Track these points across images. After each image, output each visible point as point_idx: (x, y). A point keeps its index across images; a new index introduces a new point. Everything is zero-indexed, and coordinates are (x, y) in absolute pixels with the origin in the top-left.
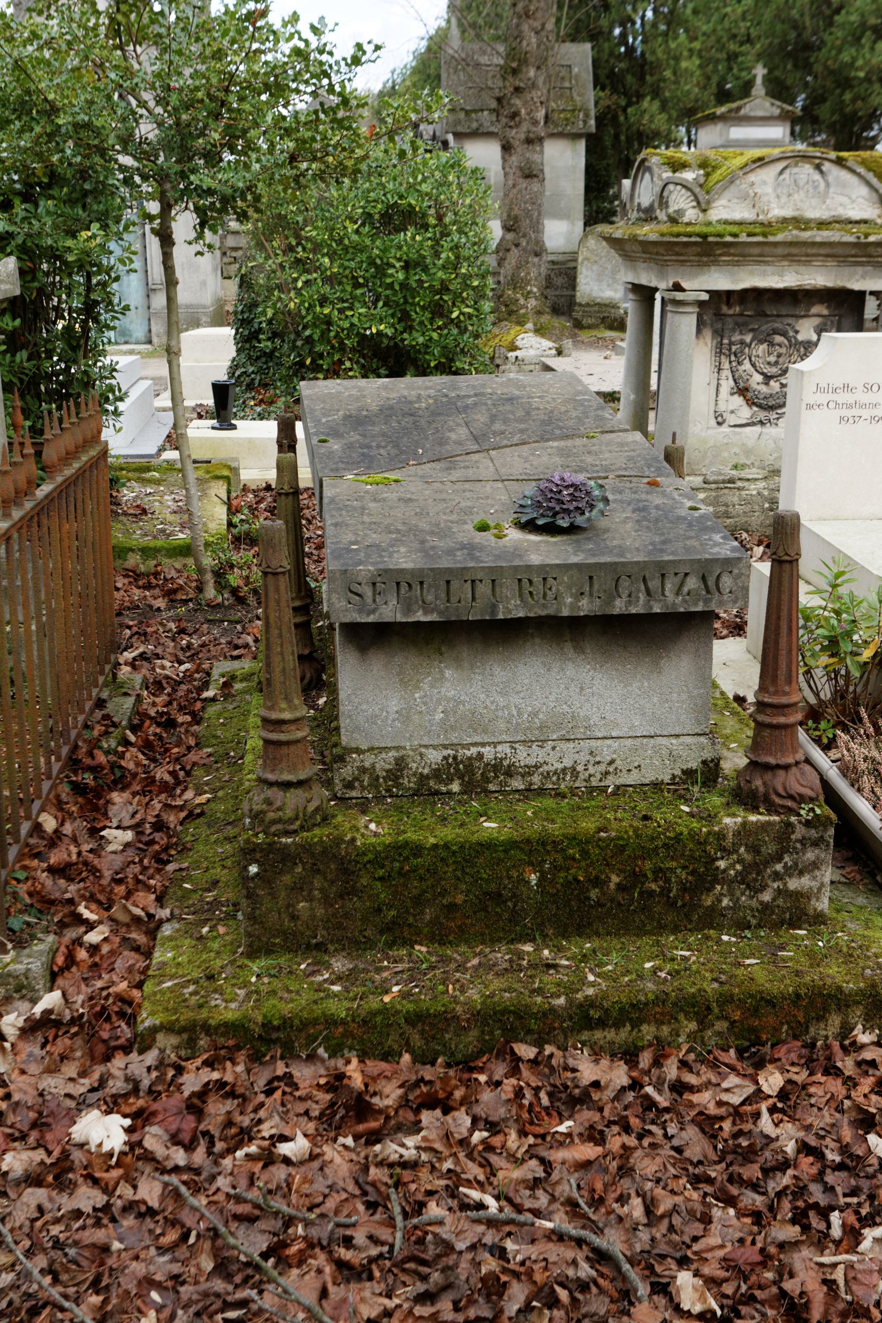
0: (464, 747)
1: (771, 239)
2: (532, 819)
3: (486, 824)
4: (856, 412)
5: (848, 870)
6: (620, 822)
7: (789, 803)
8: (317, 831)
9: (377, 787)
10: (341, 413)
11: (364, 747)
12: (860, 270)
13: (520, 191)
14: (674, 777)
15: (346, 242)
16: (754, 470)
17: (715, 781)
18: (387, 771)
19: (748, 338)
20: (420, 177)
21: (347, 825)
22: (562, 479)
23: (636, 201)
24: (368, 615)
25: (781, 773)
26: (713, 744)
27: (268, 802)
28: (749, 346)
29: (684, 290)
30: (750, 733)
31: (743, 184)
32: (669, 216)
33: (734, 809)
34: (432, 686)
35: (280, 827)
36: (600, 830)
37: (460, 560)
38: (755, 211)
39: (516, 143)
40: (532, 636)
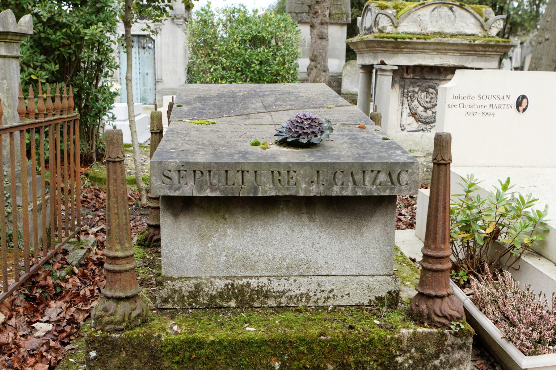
0: (238, 278)
1: (428, 41)
2: (279, 327)
3: (248, 329)
4: (474, 110)
5: (478, 362)
6: (335, 330)
7: (444, 321)
8: (137, 330)
9: (183, 302)
10: (196, 96)
11: (175, 276)
12: (471, 58)
13: (318, 44)
14: (370, 301)
15: (233, 51)
16: (419, 153)
17: (396, 305)
18: (189, 292)
19: (416, 89)
20: (268, 24)
21: (158, 326)
22: (304, 115)
23: (364, 26)
24: (175, 191)
25: (439, 301)
26: (395, 281)
27: (106, 310)
28: (417, 94)
29: (386, 65)
30: (418, 276)
31: (414, 16)
32: (379, 30)
33: (408, 323)
34: (219, 240)
35: (112, 326)
36: (321, 334)
37: (236, 158)
38: (420, 28)
39: (316, 24)
40: (282, 209)
